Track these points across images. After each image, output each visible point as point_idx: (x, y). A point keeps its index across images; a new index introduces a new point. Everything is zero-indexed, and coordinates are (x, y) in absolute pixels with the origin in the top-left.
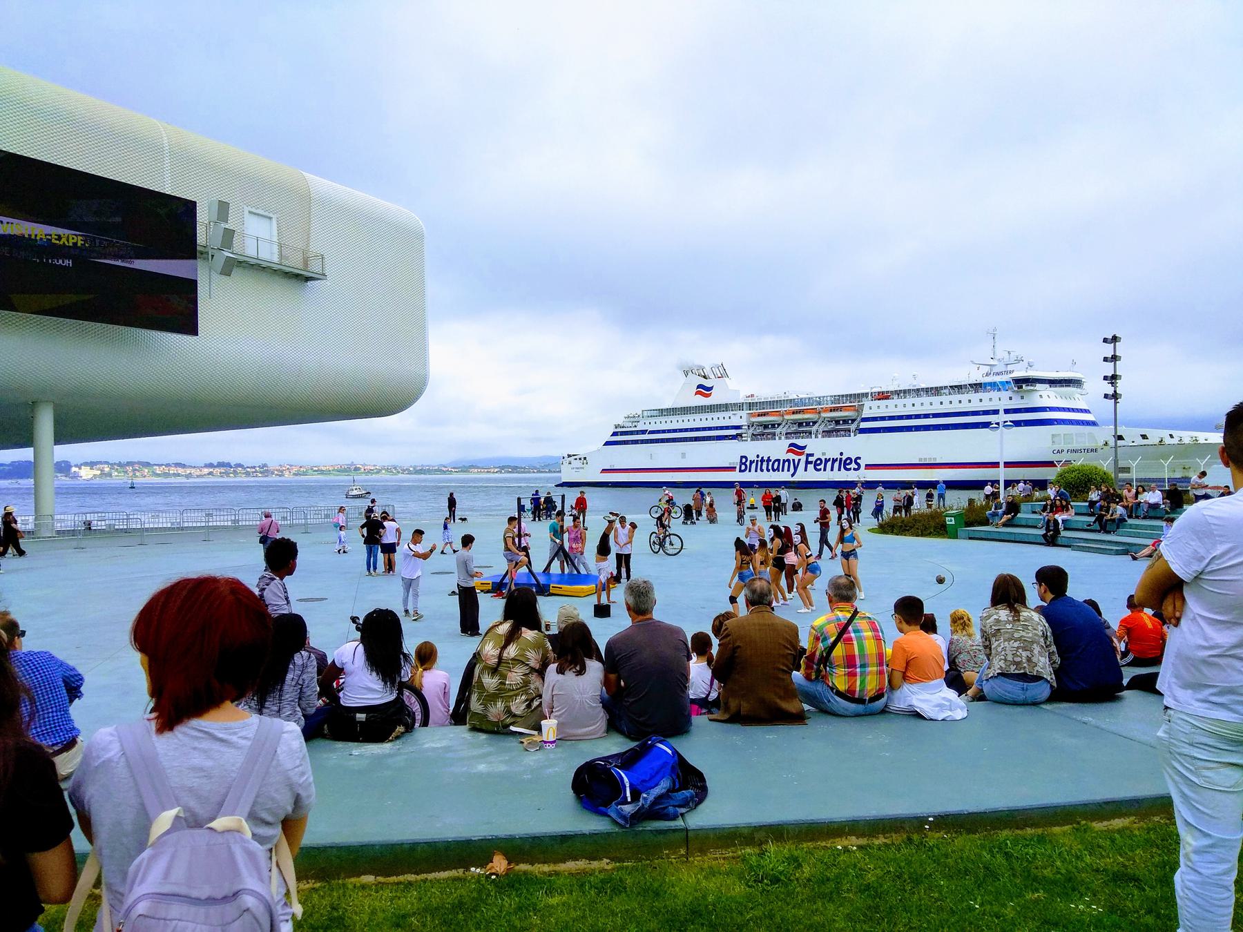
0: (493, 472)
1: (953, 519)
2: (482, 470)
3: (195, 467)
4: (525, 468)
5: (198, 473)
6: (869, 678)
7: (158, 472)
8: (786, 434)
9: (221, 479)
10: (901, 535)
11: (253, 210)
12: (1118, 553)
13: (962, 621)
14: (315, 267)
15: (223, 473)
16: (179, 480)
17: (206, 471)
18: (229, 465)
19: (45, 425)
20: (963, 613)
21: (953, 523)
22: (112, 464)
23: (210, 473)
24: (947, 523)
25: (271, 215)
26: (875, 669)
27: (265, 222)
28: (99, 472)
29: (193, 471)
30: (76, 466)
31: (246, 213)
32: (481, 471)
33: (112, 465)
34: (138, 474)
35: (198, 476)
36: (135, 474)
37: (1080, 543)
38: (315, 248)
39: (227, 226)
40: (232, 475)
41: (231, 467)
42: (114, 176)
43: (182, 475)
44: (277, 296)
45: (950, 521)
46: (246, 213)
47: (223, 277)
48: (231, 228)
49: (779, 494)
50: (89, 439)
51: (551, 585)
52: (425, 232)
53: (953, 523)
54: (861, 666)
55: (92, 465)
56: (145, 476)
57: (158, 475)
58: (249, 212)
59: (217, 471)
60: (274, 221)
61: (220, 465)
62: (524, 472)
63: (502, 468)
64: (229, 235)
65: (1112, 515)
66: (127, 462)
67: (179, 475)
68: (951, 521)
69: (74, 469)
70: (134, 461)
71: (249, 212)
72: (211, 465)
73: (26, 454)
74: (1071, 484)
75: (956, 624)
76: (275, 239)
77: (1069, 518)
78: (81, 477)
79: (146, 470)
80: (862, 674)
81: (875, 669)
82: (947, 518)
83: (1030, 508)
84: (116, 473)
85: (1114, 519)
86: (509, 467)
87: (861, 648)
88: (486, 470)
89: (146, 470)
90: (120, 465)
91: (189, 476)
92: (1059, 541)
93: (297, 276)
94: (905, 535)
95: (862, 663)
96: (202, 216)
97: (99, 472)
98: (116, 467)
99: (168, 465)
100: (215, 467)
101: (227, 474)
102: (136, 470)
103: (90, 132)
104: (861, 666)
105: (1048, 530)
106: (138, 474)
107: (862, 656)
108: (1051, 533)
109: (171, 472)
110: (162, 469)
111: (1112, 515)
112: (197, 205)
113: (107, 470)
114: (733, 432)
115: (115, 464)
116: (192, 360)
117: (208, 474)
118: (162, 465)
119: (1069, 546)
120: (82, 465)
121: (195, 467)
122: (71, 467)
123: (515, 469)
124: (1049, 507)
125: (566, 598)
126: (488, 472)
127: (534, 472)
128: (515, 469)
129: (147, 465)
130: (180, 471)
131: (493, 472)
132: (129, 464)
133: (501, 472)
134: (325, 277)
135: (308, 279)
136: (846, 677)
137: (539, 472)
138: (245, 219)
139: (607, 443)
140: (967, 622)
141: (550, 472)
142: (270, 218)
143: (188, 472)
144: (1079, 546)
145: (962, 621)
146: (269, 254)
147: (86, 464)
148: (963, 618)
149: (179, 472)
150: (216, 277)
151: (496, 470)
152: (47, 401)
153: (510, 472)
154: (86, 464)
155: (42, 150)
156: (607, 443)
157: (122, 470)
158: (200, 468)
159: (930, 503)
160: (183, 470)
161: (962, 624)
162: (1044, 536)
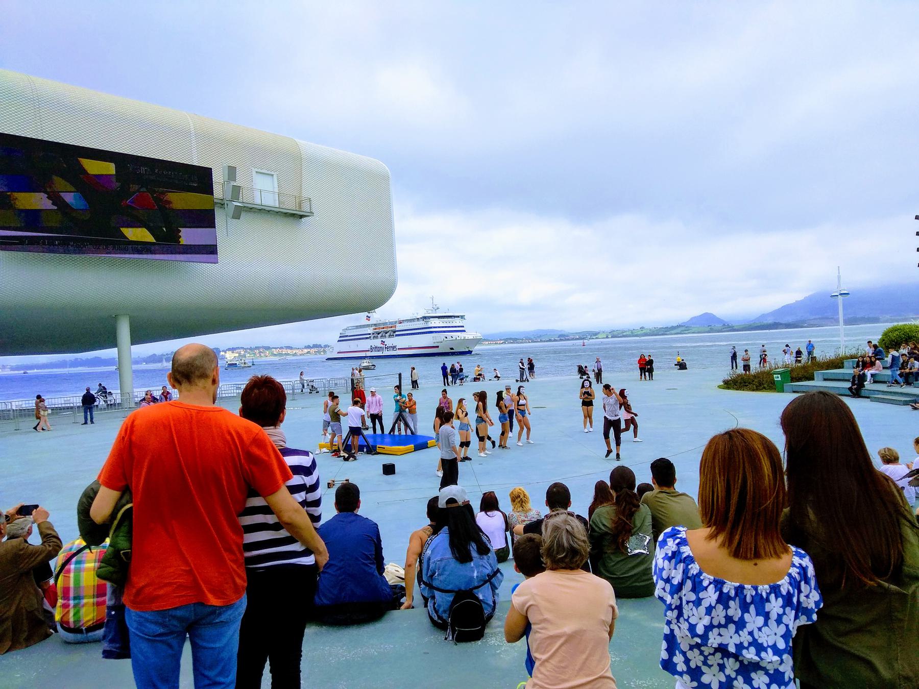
0: (500, 343)
1: (779, 376)
2: (492, 343)
3: (298, 348)
4: (522, 340)
5: (301, 352)
6: (83, 610)
7: (275, 353)
8: (389, 336)
9: (316, 356)
10: (741, 390)
11: (259, 170)
12: (906, 403)
13: (519, 499)
14: (306, 208)
15: (317, 352)
16: (289, 358)
17: (306, 351)
18: (320, 346)
19: (124, 332)
20: (519, 491)
21: (780, 379)
22: (245, 349)
23: (308, 352)
24: (775, 379)
25: (272, 173)
26: (91, 600)
27: (269, 178)
28: (237, 355)
29: (297, 351)
30: (223, 351)
31: (254, 173)
32: (490, 343)
33: (245, 349)
34: (262, 355)
35: (301, 355)
36: (260, 355)
37: (878, 394)
38: (305, 194)
39: (235, 184)
40: (322, 353)
41: (322, 348)
42: (141, 154)
43: (291, 355)
44: (279, 230)
45: (777, 378)
46: (254, 173)
47: (234, 220)
48: (238, 185)
49: (651, 358)
50: (143, 341)
51: (378, 446)
52: (390, 176)
53: (780, 379)
54: (75, 598)
55: (233, 350)
56: (267, 356)
57: (275, 355)
58: (256, 172)
59: (313, 350)
60: (275, 177)
61: (315, 346)
62: (521, 343)
63: (507, 340)
64: (237, 190)
65: (911, 369)
66: (256, 347)
67: (288, 354)
68: (778, 378)
69: (222, 353)
70: (259, 346)
71: (256, 172)
72: (308, 347)
73: (112, 353)
74: (894, 341)
75: (515, 503)
76: (276, 190)
77: (877, 372)
78: (227, 358)
79: (268, 352)
80: (75, 606)
81: (91, 600)
82: (775, 376)
83: (851, 364)
84: (249, 355)
85: (912, 372)
86: (511, 339)
87: (77, 580)
88: (494, 342)
89: (268, 352)
90: (251, 349)
91: (295, 355)
92: (863, 393)
93: (293, 215)
94: (743, 390)
95: (76, 595)
96: (218, 178)
97: (237, 355)
98: (248, 351)
99: (281, 348)
100: (312, 348)
101: (319, 352)
102: (261, 352)
103: (142, 127)
104: (75, 598)
105: (853, 384)
106: (262, 355)
107: (78, 588)
108: (856, 386)
109: (283, 353)
110: (277, 351)
111: (911, 369)
112: (213, 170)
113: (242, 353)
114: (368, 336)
115: (248, 348)
116: (202, 278)
117: (307, 353)
118: (278, 348)
119: (868, 398)
120: (227, 350)
121: (298, 348)
122: (220, 352)
123: (515, 340)
124: (861, 363)
125: (384, 455)
126: (496, 343)
127: (529, 342)
128: (515, 340)
129: (268, 348)
130: (289, 351)
131: (500, 343)
132: (257, 348)
133: (505, 343)
134: (312, 214)
135: (301, 217)
136: (95, 607)
137: (533, 342)
138: (253, 180)
139: (339, 341)
140: (523, 499)
141: (541, 341)
142: (272, 175)
143: (294, 352)
144: (876, 398)
145: (519, 499)
146: (270, 201)
147: (229, 349)
148: (519, 497)
149: (289, 352)
150: (230, 221)
151: (502, 342)
152: (124, 314)
153: (512, 343)
154: (229, 349)
155: (93, 141)
156: (339, 341)
157: (252, 353)
158: (302, 349)
159: (799, 359)
160: (291, 351)
161: (519, 502)
162: (850, 389)
